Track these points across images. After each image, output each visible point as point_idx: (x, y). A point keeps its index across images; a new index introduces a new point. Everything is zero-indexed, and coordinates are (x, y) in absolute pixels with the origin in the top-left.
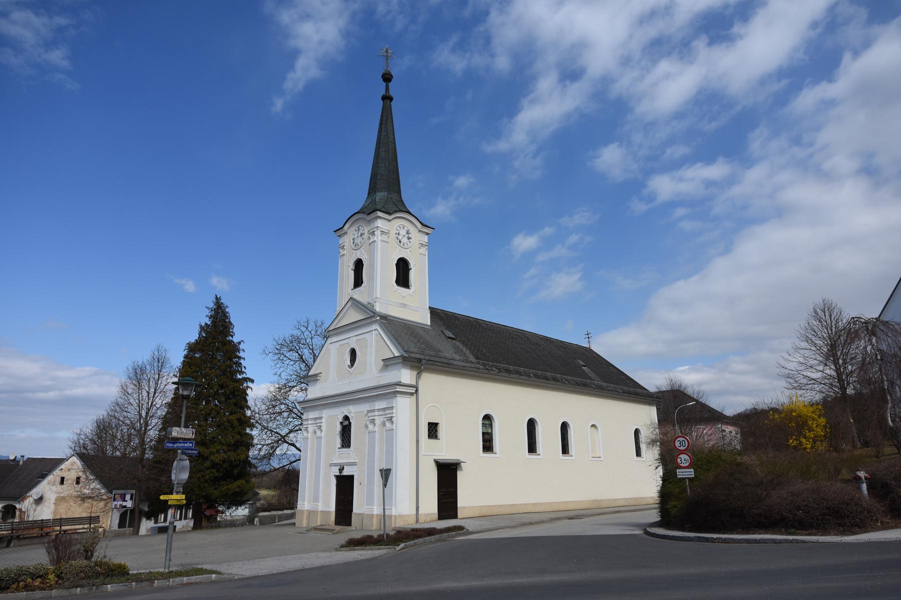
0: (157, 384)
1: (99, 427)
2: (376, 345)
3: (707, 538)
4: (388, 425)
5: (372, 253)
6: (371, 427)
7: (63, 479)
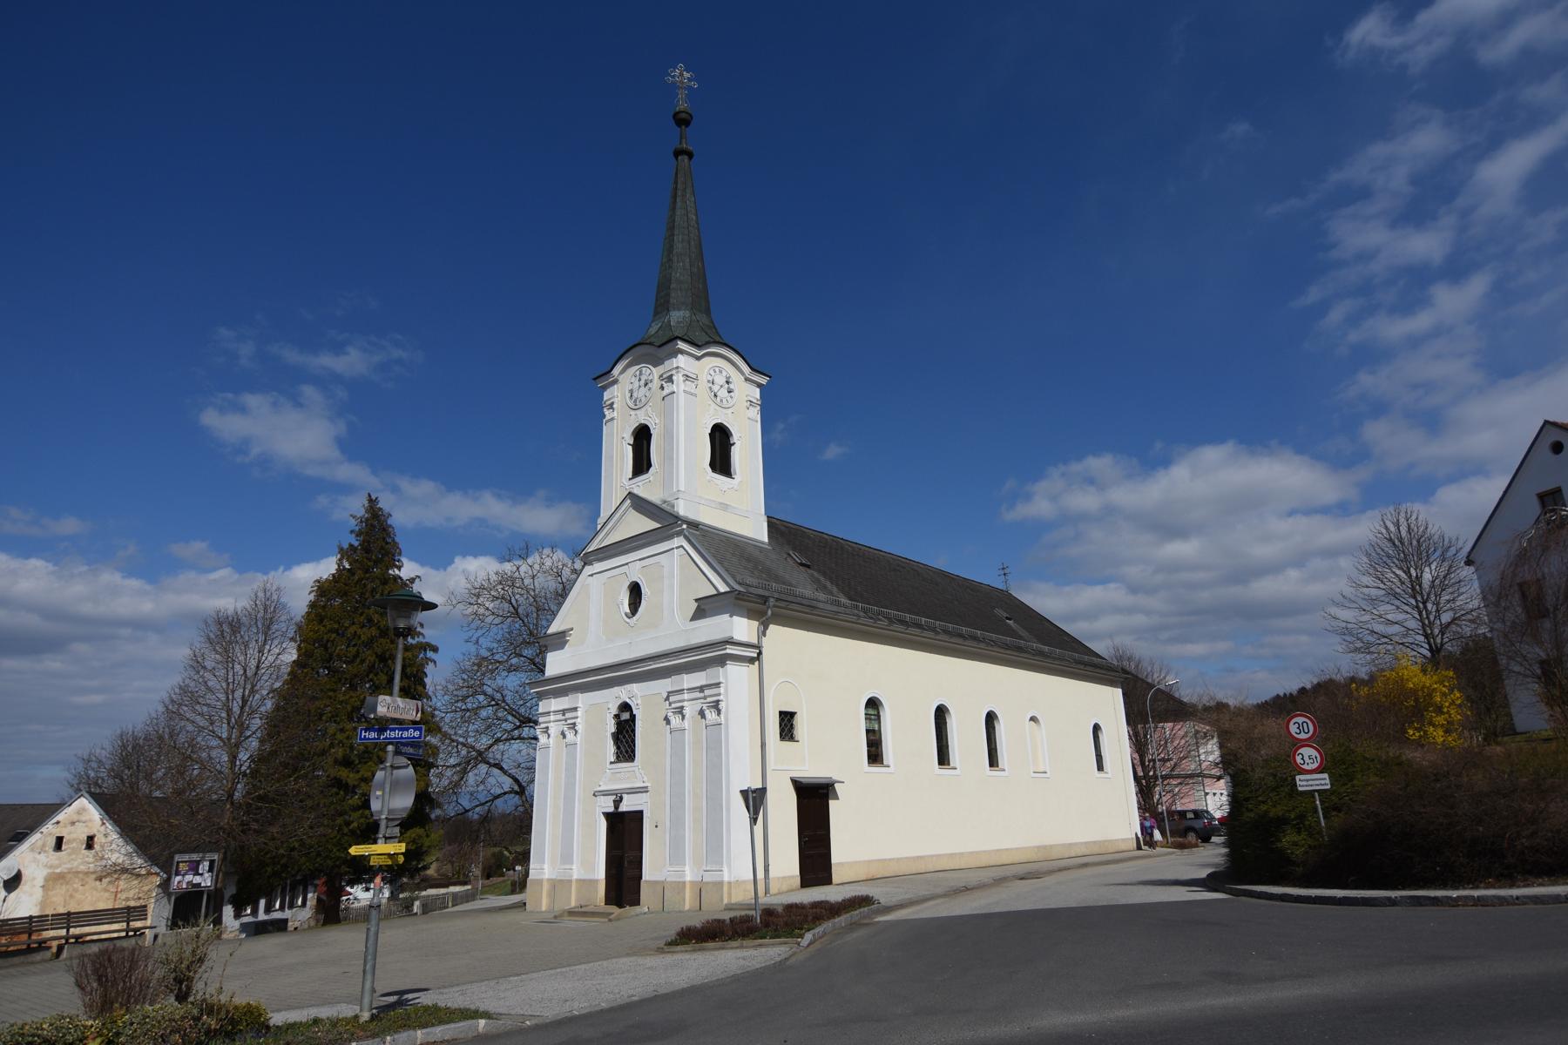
0: (261, 651)
1: (124, 747)
2: (678, 576)
3: (1436, 898)
4: (711, 715)
5: (668, 415)
6: (675, 721)
7: (60, 840)
